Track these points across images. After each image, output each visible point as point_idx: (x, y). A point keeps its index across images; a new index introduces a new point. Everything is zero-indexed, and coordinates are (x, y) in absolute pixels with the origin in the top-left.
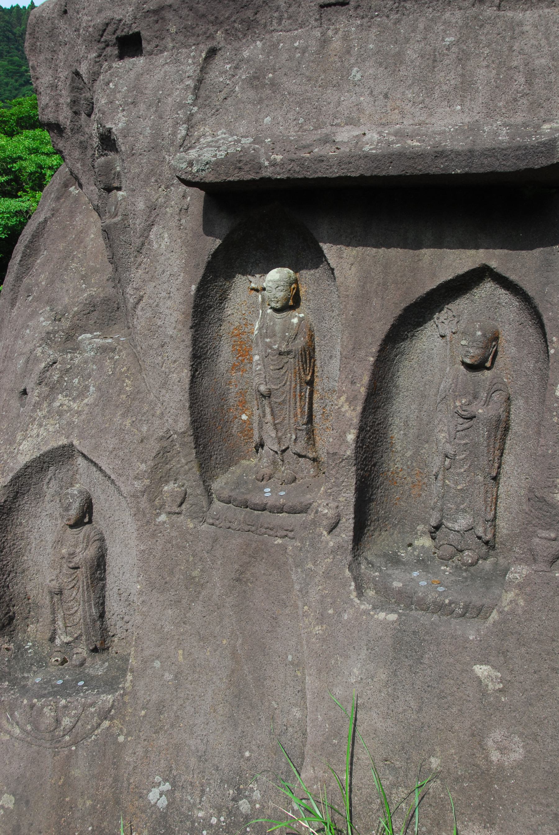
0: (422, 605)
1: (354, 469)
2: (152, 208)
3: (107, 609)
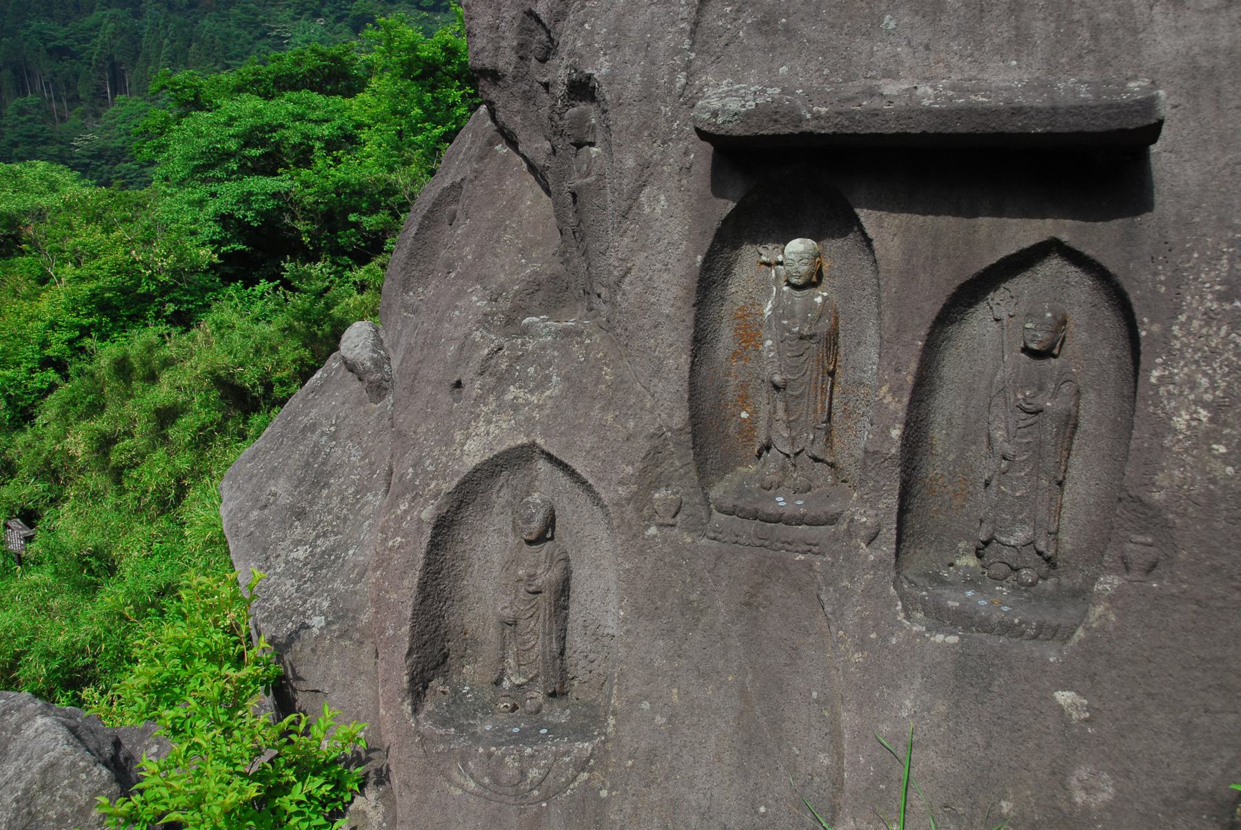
0: (985, 626)
1: (898, 470)
2: (645, 166)
3: (567, 645)
